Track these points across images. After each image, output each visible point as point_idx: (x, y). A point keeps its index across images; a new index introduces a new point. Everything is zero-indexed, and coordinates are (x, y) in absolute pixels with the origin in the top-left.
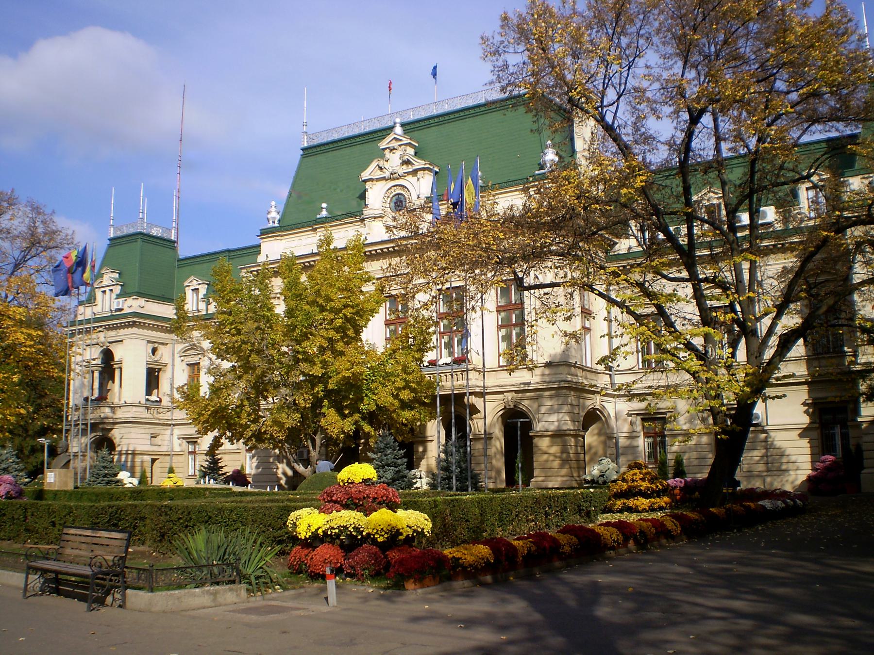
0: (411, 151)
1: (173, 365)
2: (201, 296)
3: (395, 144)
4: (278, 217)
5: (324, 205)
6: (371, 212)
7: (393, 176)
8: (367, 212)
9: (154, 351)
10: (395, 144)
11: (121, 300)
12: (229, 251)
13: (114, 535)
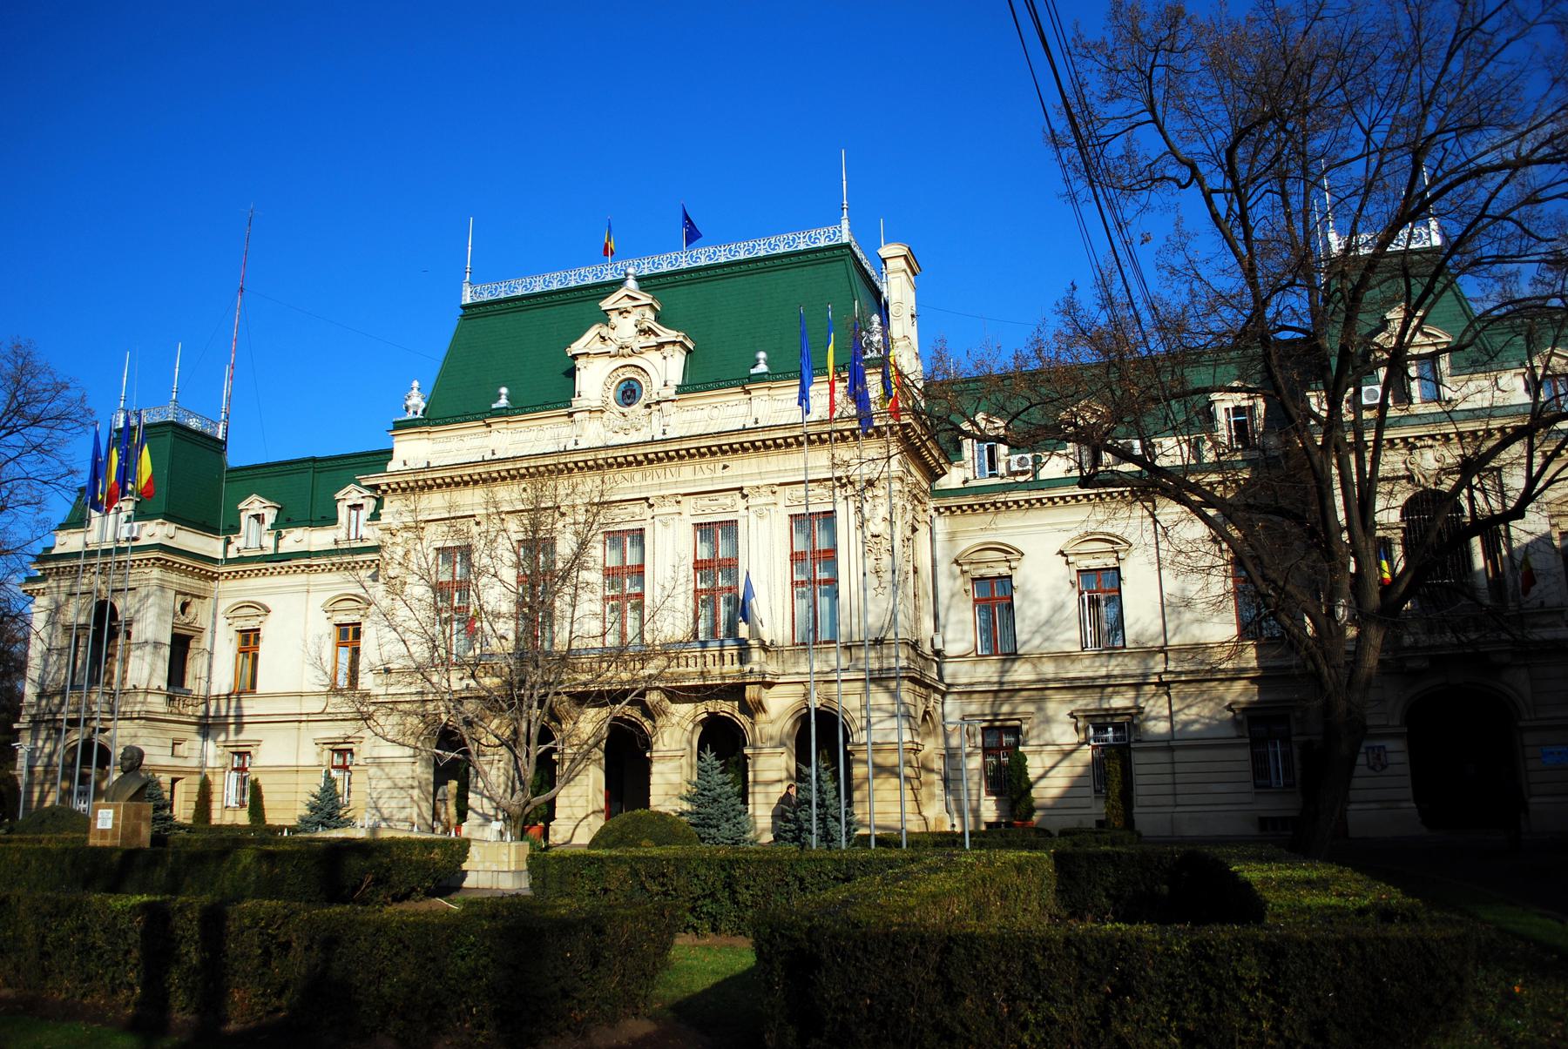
0: (650, 315)
1: (214, 632)
2: (267, 525)
3: (627, 304)
4: (423, 405)
5: (504, 390)
6: (586, 403)
7: (624, 350)
8: (577, 403)
9: (184, 606)
10: (627, 304)
11: (136, 525)
12: (314, 460)
13: (1547, 634)
